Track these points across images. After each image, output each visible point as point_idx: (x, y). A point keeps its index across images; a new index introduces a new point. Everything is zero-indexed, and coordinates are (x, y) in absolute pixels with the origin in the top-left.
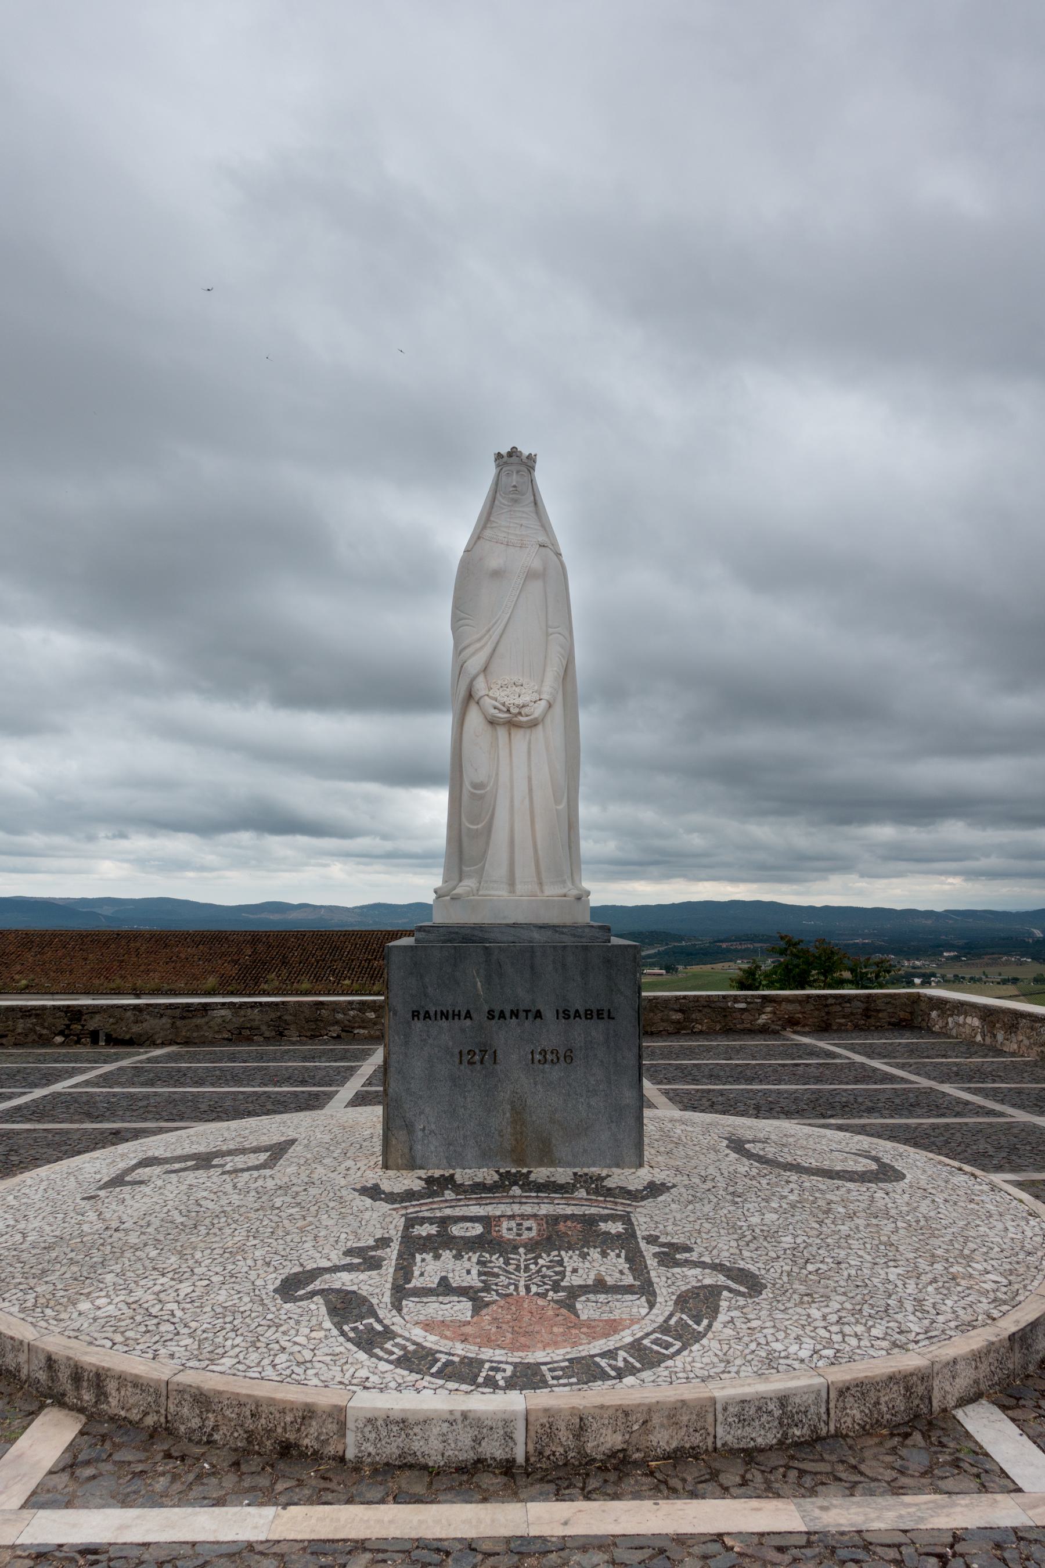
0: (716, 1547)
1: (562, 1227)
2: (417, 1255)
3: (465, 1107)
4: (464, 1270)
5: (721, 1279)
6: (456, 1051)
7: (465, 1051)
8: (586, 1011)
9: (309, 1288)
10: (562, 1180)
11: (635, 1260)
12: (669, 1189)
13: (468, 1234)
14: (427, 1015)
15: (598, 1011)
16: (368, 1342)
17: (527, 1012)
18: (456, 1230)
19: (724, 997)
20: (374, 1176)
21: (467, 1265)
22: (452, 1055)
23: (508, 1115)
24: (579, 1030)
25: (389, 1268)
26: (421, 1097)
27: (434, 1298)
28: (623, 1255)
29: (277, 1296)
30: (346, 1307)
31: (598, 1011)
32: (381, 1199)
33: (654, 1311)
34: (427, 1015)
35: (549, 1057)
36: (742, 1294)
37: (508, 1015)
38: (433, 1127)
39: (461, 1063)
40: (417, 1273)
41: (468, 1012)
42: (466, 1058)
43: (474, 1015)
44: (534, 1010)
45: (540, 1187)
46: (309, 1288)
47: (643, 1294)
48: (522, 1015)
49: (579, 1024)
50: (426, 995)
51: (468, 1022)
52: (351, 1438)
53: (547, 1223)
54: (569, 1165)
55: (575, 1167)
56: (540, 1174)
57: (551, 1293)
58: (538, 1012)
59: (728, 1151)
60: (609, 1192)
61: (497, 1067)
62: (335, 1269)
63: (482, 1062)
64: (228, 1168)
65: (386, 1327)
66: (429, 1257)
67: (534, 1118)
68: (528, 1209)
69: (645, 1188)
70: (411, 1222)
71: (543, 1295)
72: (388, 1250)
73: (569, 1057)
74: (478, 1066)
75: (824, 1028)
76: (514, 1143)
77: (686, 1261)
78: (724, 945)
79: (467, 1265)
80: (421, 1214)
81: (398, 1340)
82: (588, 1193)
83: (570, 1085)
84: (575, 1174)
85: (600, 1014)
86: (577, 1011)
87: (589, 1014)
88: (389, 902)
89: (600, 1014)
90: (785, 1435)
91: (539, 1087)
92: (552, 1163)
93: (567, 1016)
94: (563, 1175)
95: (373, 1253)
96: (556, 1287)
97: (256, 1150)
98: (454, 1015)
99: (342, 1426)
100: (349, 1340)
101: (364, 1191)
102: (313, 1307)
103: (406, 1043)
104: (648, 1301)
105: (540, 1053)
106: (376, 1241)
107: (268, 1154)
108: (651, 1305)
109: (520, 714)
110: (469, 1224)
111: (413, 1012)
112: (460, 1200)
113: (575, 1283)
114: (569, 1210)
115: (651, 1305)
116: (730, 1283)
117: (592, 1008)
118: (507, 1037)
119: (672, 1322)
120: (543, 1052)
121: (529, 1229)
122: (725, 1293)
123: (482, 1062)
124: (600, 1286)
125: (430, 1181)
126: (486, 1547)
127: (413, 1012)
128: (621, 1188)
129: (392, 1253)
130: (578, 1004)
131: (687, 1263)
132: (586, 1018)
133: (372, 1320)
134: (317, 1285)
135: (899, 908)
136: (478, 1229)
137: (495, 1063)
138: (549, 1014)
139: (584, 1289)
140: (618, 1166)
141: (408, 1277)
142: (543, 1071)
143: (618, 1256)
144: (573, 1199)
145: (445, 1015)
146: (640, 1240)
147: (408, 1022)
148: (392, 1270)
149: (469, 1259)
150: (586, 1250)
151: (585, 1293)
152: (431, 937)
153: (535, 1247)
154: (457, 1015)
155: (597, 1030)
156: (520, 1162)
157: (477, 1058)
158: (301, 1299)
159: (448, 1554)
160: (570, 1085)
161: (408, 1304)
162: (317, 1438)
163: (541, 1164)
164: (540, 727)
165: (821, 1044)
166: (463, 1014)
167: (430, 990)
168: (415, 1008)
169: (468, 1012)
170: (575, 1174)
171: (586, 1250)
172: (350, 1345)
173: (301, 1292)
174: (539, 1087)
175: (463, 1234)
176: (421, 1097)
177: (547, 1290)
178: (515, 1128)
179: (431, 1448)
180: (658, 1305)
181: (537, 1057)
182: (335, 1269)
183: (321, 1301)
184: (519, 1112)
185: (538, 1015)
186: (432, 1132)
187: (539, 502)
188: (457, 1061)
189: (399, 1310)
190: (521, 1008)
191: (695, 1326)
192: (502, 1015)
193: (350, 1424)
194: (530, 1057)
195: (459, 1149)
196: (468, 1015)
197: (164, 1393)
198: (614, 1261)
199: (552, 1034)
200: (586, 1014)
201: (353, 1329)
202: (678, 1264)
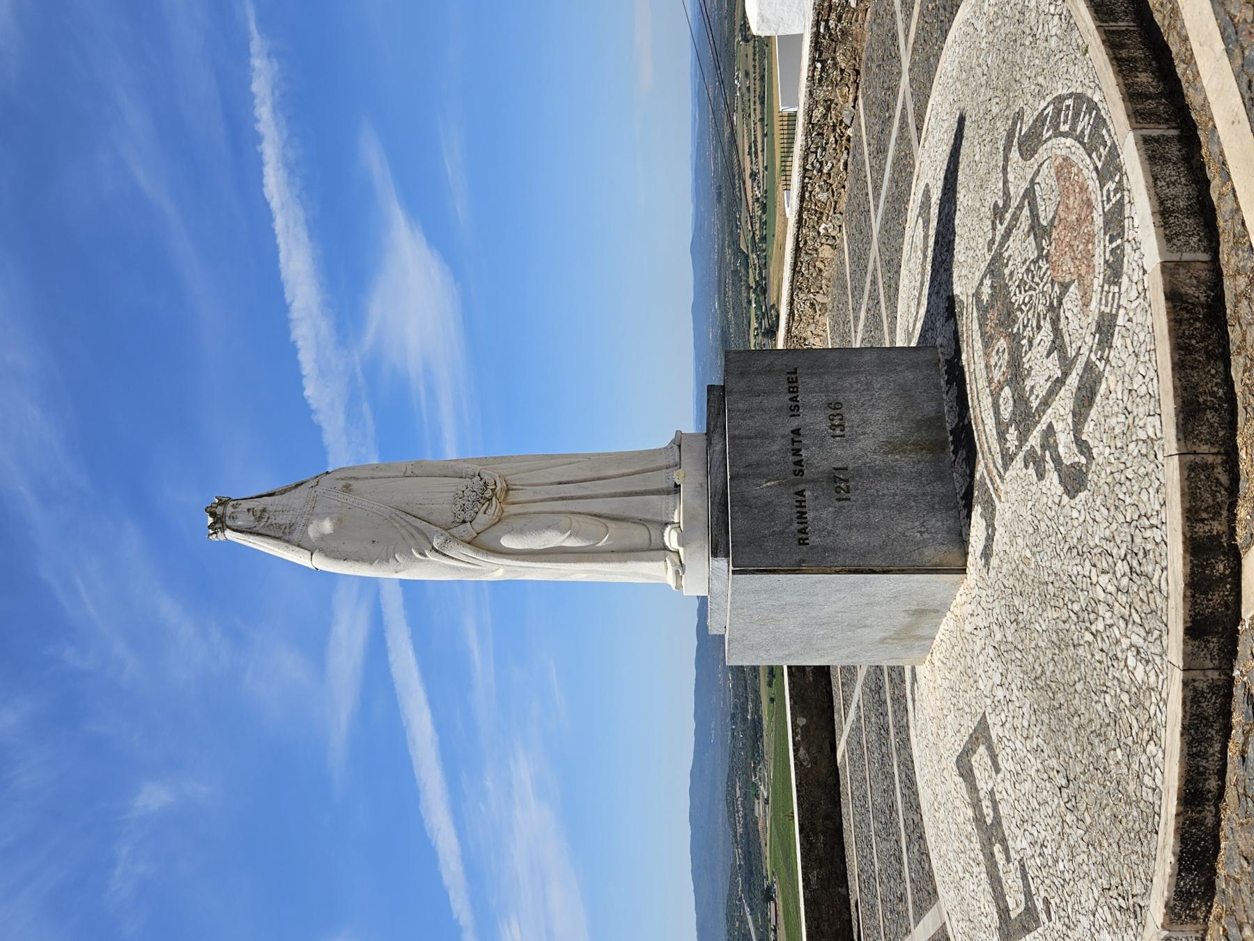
7: (838, 496)
17: (793, 442)
22: (843, 507)
34: (802, 531)
37: (797, 458)
39: (849, 499)
41: (797, 493)
42: (843, 494)
43: (801, 487)
48: (796, 446)
50: (782, 532)
51: (807, 493)
58: (793, 432)
61: (851, 466)
63: (846, 481)
73: (835, 406)
78: (740, 830)
83: (863, 405)
86: (791, 399)
87: (793, 389)
88: (694, 682)
98: (801, 506)
99: (1178, 264)
101: (987, 563)
103: (833, 550)
120: (833, 427)
123: (846, 481)
135: (694, 725)
137: (846, 469)
138: (795, 423)
142: (852, 427)
145: (802, 515)
147: (812, 548)
157: (843, 485)
160: (863, 405)
162: (1197, 287)
166: (799, 498)
169: (797, 493)
174: (868, 431)
179: (1181, 193)
181: (838, 432)
185: (796, 432)
186: (922, 525)
188: (846, 503)
190: (790, 447)
193: (1176, 257)
196: (801, 493)
197: (1192, 457)
199: (815, 420)
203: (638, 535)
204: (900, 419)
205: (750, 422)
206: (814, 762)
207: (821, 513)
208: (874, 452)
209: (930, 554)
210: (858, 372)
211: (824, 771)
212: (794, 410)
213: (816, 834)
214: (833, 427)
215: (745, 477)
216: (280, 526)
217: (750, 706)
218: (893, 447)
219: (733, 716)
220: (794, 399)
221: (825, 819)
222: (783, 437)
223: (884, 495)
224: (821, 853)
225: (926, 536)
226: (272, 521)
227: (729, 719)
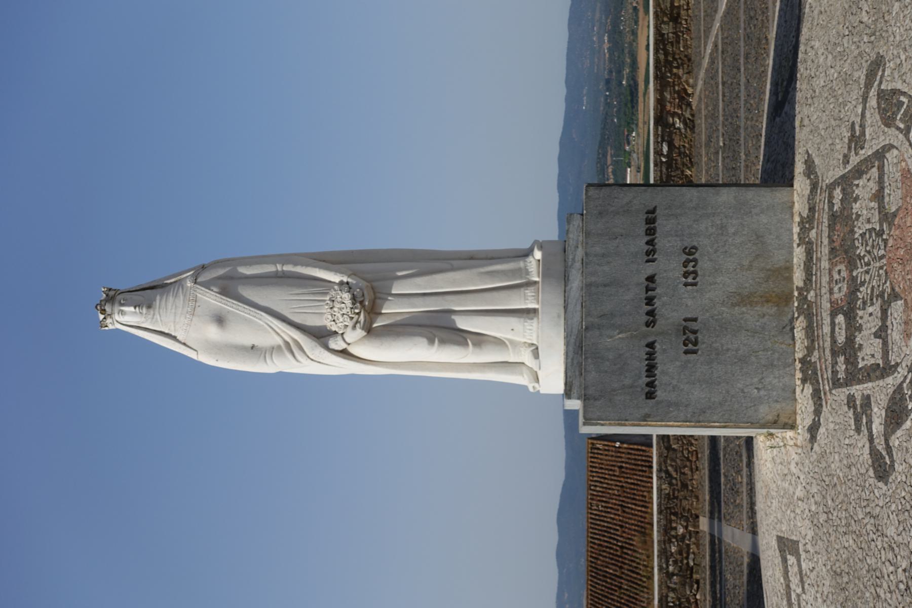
1: (837, 244)
2: (860, 366)
3: (737, 350)
4: (869, 318)
5: (873, 92)
6: (684, 357)
8: (647, 234)
9: (884, 453)
10: (803, 257)
11: (859, 172)
12: (809, 155)
13: (844, 326)
15: (647, 224)
17: (648, 289)
18: (841, 339)
19: (656, 165)
20: (800, 435)
21: (866, 317)
23: (744, 309)
26: (728, 392)
27: (889, 337)
28: (856, 182)
29: (890, 480)
31: (647, 224)
32: (819, 420)
33: (895, 144)
34: (651, 384)
36: (884, 71)
38: (756, 380)
40: (872, 361)
43: (651, 340)
44: (646, 283)
45: (808, 279)
46: (884, 453)
47: (884, 156)
49: (661, 242)
51: (658, 346)
53: (835, 258)
54: (791, 253)
55: (793, 247)
56: (798, 278)
57: (884, 237)
59: (783, 115)
60: (812, 209)
62: (871, 439)
64: (799, 591)
67: (747, 285)
68: (825, 279)
69: (809, 177)
70: (836, 383)
71: (885, 242)
72: (856, 395)
73: (690, 251)
75: (688, 63)
76: (770, 304)
77: (861, 126)
79: (866, 317)
80: (830, 376)
82: (813, 228)
83: (716, 251)
84: (799, 245)
87: (651, 232)
91: (719, 280)
92: (789, 269)
93: (654, 251)
94: (799, 254)
95: (859, 407)
96: (880, 233)
97: (785, 560)
101: (813, 439)
102: (897, 443)
104: (889, 150)
105: (686, 278)
106: (849, 407)
107: (789, 557)
108: (892, 146)
109: (361, 303)
110: (837, 329)
111: (647, 398)
112: (819, 347)
113: (877, 218)
114: (826, 241)
115: (892, 146)
116: (876, 83)
117: (644, 229)
118: (671, 313)
119: (902, 126)
121: (839, 272)
122: (882, 87)
124: (879, 196)
125: (804, 381)
127: (647, 398)
128: (809, 199)
130: (641, 243)
131: (862, 126)
132: (654, 234)
133: (905, 385)
134: (881, 448)
136: (840, 319)
138: (650, 269)
139: (881, 208)
140: (792, 207)
143: (857, 185)
144: (817, 240)
146: (847, 170)
147: (658, 403)
149: (861, 318)
150: (854, 216)
151: (884, 207)
152: (576, 383)
153: (851, 265)
154: (651, 356)
155: (663, 225)
156: (788, 298)
157: (692, 337)
158: (893, 461)
161: (893, 358)
163: (790, 279)
164: (375, 284)
165: (706, 62)
167: (627, 382)
168: (644, 397)
170: (799, 245)
171: (854, 216)
173: (888, 461)
175: (844, 331)
176: (728, 392)
177: (883, 240)
178: (757, 303)
180: (891, 142)
181: (690, 280)
182: (871, 439)
183: (893, 437)
184: (744, 299)
185: (651, 279)
186: (760, 382)
187: (152, 285)
189: (897, 364)
190: (644, 295)
191: (905, 106)
192: (651, 313)
194: (689, 288)
195: (776, 355)
196: (651, 345)
198: (861, 189)
199: (669, 267)
200: (650, 235)
202: (863, 133)
205: (606, 268)
207: (670, 365)
208: (723, 304)
210: (714, 215)
212: (651, 254)
214: (686, 275)
215: (599, 327)
217: (627, 71)
219: (608, 82)
220: (650, 243)
222: (638, 284)
223: (728, 350)
225: (762, 393)
227: (602, 86)
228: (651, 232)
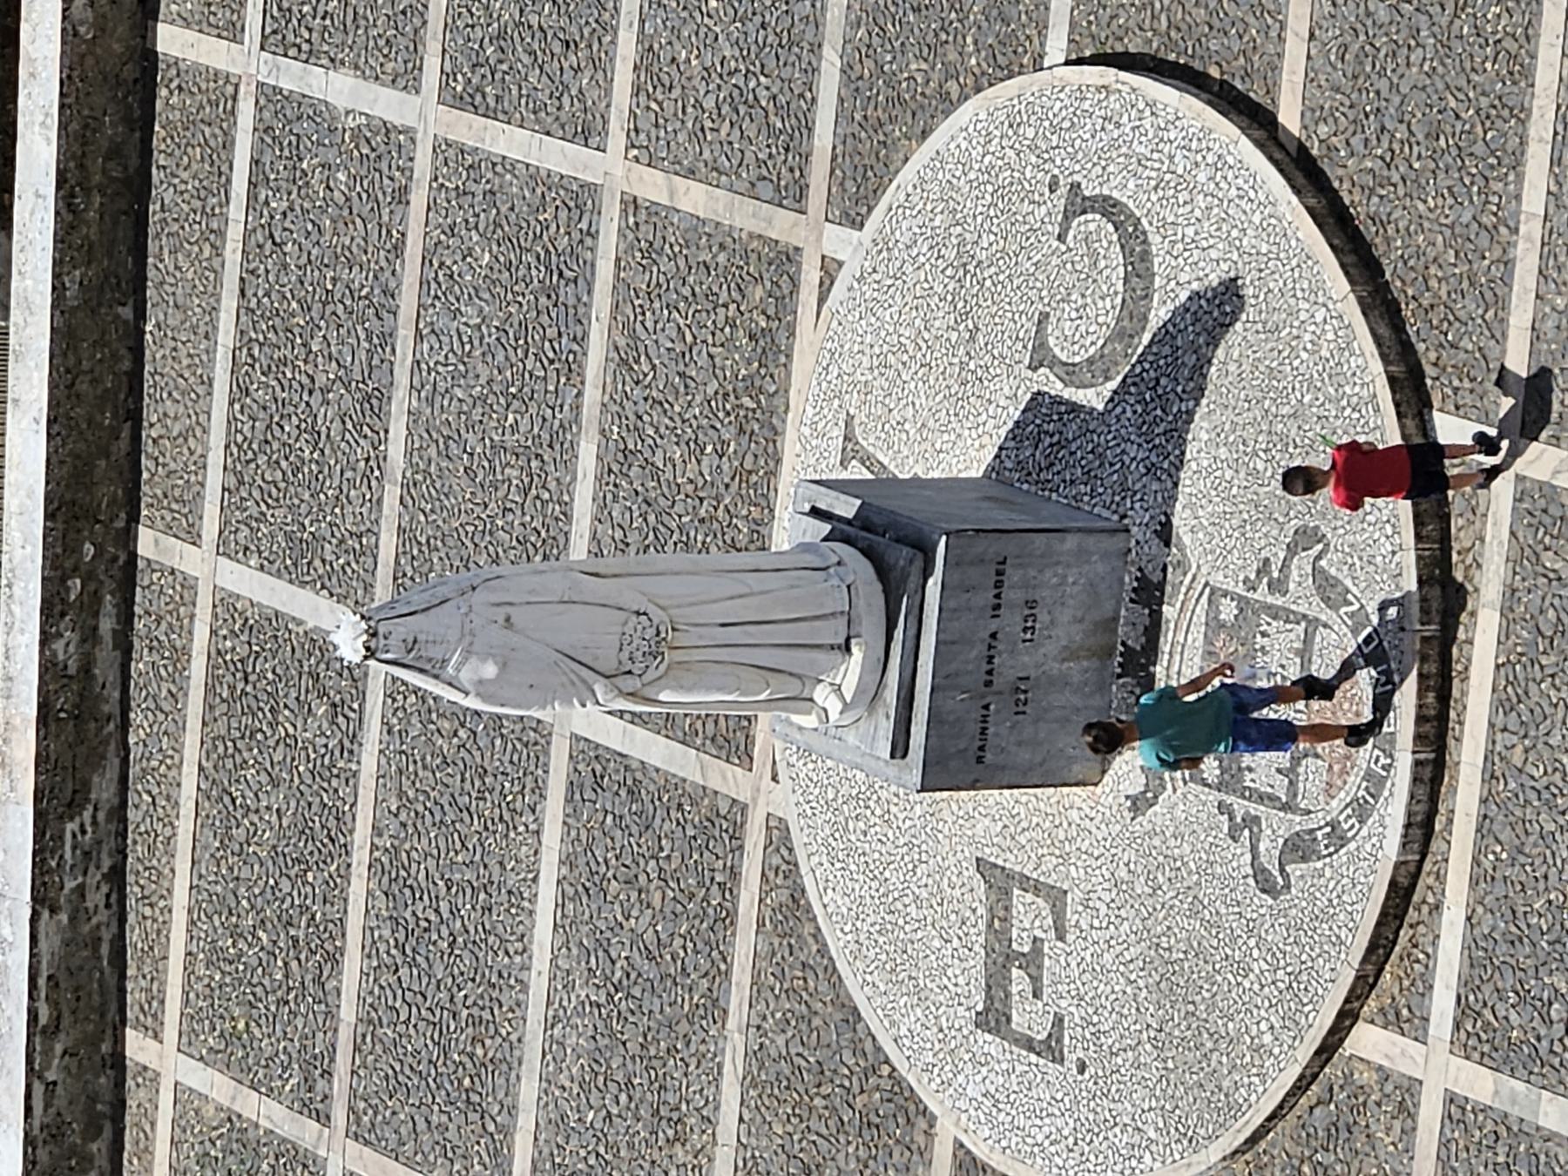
0: (1502, 671)
14: (981, 748)
16: (1338, 837)
17: (990, 647)
24: (1011, 595)
25: (1255, 809)
30: (1299, 848)
34: (981, 748)
35: (1029, 624)
43: (985, 702)
46: (1276, 873)
49: (1008, 594)
50: (966, 750)
52: (1410, 858)
61: (1033, 676)
62: (1254, 849)
63: (1025, 692)
65: (1327, 824)
66: (1248, 776)
73: (1031, 604)
74: (1030, 695)
81: (1341, 818)
85: (999, 573)
87: (999, 584)
89: (999, 573)
90: (1438, 582)
93: (997, 607)
99: (1403, 863)
100: (1337, 851)
118: (1009, 667)
120: (1025, 630)
122: (1323, 563)
126: (1485, 793)
129: (1241, 807)
137: (1027, 678)
138: (994, 625)
141: (1272, 798)
148: (1262, 808)
155: (1013, 575)
157: (1022, 697)
159: (1485, 816)
167: (962, 747)
172: (1342, 851)
182: (1254, 849)
185: (993, 636)
192: (990, 673)
196: (986, 707)
199: (1011, 622)
201: (1327, 847)
203: (793, 687)
204: (1081, 621)
205: (956, 624)
206: (101, 27)
208: (1054, 659)
209: (1077, 771)
211: (117, 47)
213: (87, 192)
216: (430, 660)
218: (1070, 654)
220: (998, 596)
221: (107, 159)
222: (983, 641)
224: (93, 233)
226: (423, 653)
228: (999, 584)
